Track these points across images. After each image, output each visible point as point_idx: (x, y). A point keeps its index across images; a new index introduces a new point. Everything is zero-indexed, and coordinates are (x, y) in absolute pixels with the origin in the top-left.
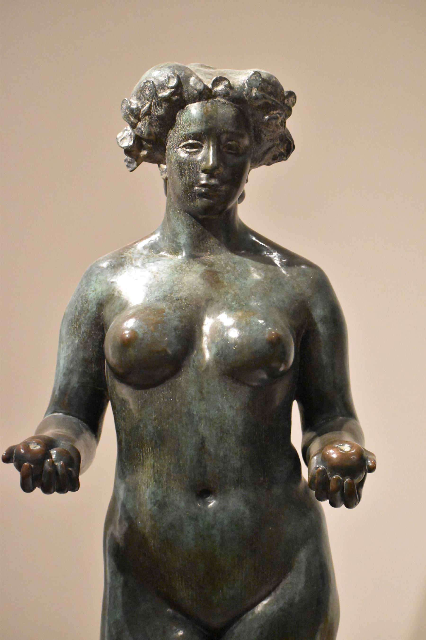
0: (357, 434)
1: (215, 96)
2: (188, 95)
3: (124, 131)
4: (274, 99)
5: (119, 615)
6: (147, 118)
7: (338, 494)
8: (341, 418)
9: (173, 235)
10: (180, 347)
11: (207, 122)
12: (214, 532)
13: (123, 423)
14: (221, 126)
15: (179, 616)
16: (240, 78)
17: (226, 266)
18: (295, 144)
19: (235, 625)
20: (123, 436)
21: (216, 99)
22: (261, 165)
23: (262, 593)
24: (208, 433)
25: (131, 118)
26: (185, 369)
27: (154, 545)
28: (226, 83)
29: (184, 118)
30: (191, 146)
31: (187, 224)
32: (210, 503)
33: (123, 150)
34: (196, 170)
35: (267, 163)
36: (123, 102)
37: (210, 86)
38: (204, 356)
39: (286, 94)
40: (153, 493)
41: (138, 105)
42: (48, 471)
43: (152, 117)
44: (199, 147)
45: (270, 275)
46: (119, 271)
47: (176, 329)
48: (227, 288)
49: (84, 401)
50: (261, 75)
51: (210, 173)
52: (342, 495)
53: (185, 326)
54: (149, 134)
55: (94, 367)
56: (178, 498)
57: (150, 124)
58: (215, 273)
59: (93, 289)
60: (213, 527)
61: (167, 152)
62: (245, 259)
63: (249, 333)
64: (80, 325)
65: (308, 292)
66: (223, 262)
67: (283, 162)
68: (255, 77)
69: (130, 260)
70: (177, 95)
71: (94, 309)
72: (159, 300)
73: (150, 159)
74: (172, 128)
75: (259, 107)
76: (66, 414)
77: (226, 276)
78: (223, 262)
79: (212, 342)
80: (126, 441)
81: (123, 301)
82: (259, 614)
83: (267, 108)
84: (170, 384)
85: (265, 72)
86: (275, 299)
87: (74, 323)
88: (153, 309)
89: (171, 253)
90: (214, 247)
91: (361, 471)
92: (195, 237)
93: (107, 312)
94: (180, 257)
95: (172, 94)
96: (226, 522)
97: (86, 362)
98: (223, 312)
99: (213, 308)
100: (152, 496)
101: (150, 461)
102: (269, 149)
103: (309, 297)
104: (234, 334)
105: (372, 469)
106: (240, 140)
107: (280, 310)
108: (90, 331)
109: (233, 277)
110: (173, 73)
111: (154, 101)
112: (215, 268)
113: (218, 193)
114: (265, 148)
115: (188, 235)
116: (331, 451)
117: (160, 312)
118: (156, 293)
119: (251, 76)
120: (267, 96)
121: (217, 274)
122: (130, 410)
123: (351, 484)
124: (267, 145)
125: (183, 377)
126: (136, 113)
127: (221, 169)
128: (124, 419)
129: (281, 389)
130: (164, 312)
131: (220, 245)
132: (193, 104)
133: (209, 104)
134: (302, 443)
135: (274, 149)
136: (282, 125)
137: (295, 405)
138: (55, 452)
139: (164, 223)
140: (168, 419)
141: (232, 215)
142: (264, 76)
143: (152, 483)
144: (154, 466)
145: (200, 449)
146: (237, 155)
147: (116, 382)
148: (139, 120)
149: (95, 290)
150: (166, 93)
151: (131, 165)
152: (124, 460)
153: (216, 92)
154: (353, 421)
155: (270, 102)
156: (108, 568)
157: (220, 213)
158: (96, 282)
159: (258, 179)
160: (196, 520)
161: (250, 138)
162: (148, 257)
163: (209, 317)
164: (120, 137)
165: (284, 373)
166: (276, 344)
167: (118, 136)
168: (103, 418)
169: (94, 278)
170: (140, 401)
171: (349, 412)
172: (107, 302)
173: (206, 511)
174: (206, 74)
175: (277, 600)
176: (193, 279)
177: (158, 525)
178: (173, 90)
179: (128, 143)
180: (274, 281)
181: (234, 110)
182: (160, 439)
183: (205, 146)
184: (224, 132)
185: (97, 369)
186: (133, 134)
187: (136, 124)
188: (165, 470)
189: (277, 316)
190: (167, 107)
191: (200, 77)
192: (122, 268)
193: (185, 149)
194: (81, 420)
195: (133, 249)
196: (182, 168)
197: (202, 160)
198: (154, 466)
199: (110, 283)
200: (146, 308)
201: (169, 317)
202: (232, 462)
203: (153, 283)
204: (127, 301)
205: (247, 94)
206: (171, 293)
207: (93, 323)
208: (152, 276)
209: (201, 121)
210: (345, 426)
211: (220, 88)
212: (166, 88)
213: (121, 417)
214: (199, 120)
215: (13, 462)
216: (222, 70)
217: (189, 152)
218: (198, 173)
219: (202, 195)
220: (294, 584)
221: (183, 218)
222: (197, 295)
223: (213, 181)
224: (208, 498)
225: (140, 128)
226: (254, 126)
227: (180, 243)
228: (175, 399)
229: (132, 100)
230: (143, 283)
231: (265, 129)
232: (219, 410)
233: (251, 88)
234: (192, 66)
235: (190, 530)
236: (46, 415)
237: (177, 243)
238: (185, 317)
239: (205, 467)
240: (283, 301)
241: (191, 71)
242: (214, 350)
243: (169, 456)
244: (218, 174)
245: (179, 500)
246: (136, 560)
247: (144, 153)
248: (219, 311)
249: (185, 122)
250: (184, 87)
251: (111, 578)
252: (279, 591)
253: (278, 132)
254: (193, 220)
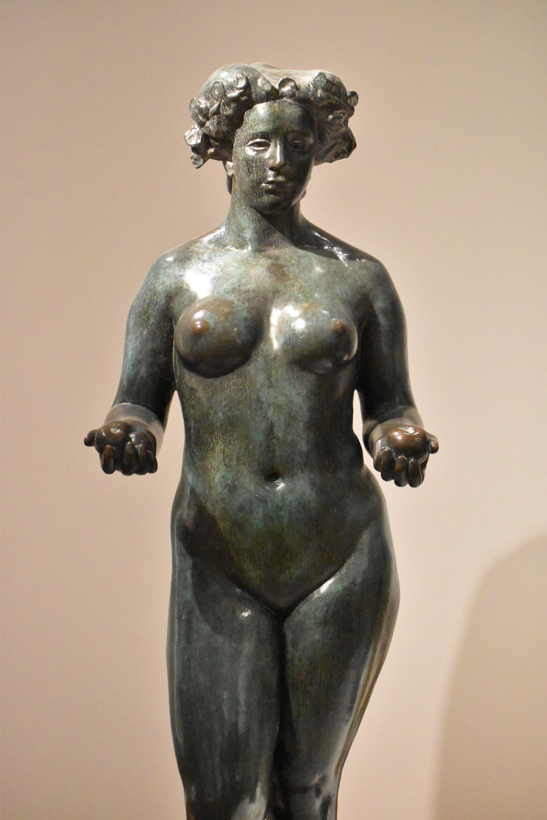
0: (416, 421)
2: (256, 95)
3: (191, 130)
4: (337, 99)
5: (189, 595)
6: (215, 117)
7: (403, 474)
8: (401, 407)
9: (239, 230)
10: (249, 337)
11: (274, 122)
12: (282, 513)
13: (192, 411)
14: (288, 125)
15: (247, 596)
16: (306, 78)
17: (291, 260)
18: (356, 142)
19: (301, 604)
20: (192, 423)
22: (323, 162)
23: (326, 574)
24: (276, 418)
25: (200, 117)
26: (254, 358)
27: (224, 527)
28: (293, 84)
29: (252, 118)
30: (259, 144)
32: (278, 486)
33: (191, 147)
35: (329, 160)
36: (192, 101)
37: (277, 87)
38: (272, 345)
39: (349, 94)
40: (223, 477)
41: (206, 105)
42: (125, 454)
43: (220, 117)
44: (266, 145)
45: (333, 268)
46: (186, 265)
47: (245, 319)
48: (292, 281)
49: (151, 390)
50: (325, 76)
51: (277, 170)
52: (407, 473)
53: (254, 317)
54: (217, 133)
55: (162, 358)
56: (248, 481)
57: (219, 123)
58: (281, 266)
59: (161, 282)
60: (281, 509)
61: (234, 149)
62: (309, 253)
63: (316, 323)
64: (148, 316)
65: (370, 285)
66: (287, 256)
67: (345, 159)
68: (320, 78)
69: (196, 255)
71: (163, 301)
72: (228, 293)
73: (216, 156)
74: (239, 127)
75: (324, 107)
76: (133, 403)
77: (291, 269)
78: (287, 256)
79: (280, 332)
80: (195, 428)
81: (192, 293)
82: (324, 593)
83: (331, 108)
84: (240, 372)
85: (328, 73)
86: (338, 291)
87: (141, 315)
88: (223, 301)
89: (237, 248)
90: (279, 241)
91: (425, 453)
93: (176, 305)
94: (245, 251)
95: (241, 95)
96: (294, 504)
97: (154, 352)
98: (289, 304)
99: (280, 300)
100: (222, 480)
101: (220, 447)
102: (332, 147)
103: (371, 290)
104: (300, 325)
105: (435, 450)
106: (305, 139)
107: (344, 302)
108: (159, 322)
109: (298, 271)
110: (242, 75)
111: (223, 101)
112: (281, 262)
113: (284, 189)
114: (327, 147)
116: (396, 433)
117: (230, 304)
118: (224, 285)
119: (316, 77)
120: (332, 96)
121: (282, 268)
122: (200, 398)
123: (415, 464)
124: (330, 143)
125: (252, 365)
126: (204, 113)
127: (288, 167)
128: (193, 407)
129: (345, 377)
130: (233, 303)
131: (284, 240)
132: (260, 104)
133: (276, 105)
134: (363, 430)
135: (337, 147)
136: (345, 125)
137: (356, 393)
138: (133, 435)
139: (229, 218)
140: (238, 406)
141: (296, 209)
142: (328, 77)
143: (222, 467)
144: (224, 450)
145: (269, 435)
146: (303, 153)
147: (186, 371)
148: (208, 119)
149: (164, 283)
150: (234, 94)
151: (198, 162)
152: (193, 446)
153: (283, 93)
154: (412, 410)
155: (334, 102)
156: (176, 552)
157: (286, 208)
158: (164, 275)
159: (322, 176)
160: (265, 501)
161: (315, 136)
162: (214, 251)
163: (277, 308)
164: (188, 135)
165: (348, 362)
166: (342, 334)
167: (186, 134)
168: (169, 407)
169: (162, 272)
170: (210, 389)
171: (408, 402)
172: (176, 295)
173: (274, 494)
174: (271, 74)
175: (342, 579)
176: (258, 273)
177: (228, 507)
179: (196, 141)
180: (337, 274)
182: (232, 424)
183: (272, 144)
184: (291, 131)
185: (165, 359)
186: (200, 132)
187: (205, 123)
188: (234, 454)
189: (341, 307)
190: (236, 107)
191: (268, 78)
192: (189, 262)
193: (252, 147)
194: (150, 409)
195: (199, 243)
196: (250, 166)
197: (269, 158)
198: (224, 450)
199: (178, 276)
200: (215, 300)
201: (238, 308)
202: (299, 446)
203: (221, 276)
204: (196, 294)
205: (313, 95)
206: (239, 286)
207: (162, 316)
208: (220, 270)
209: (269, 121)
210: (405, 414)
211: (286, 89)
212: (235, 89)
213: (190, 405)
214: (267, 120)
215: (94, 445)
216: (287, 71)
217: (256, 151)
218: (265, 170)
219: (269, 192)
220: (356, 565)
221: (249, 213)
222: (264, 287)
223: (280, 178)
224: (276, 481)
225: (208, 127)
226: (319, 125)
227: (246, 237)
228: (245, 387)
229: (200, 100)
230: (213, 276)
231: (329, 128)
232: (286, 396)
233: (316, 88)
234: (257, 66)
235: (259, 512)
236: (114, 403)
237: (242, 237)
238: (252, 308)
239: (274, 451)
240: (347, 294)
241: (258, 72)
242: (282, 340)
243: (240, 441)
244: (284, 172)
245: (249, 484)
246: (204, 542)
247: (211, 150)
248: (286, 302)
249: (253, 122)
250: (252, 88)
251: (180, 561)
252: (343, 570)
253: (341, 131)
254: (259, 215)
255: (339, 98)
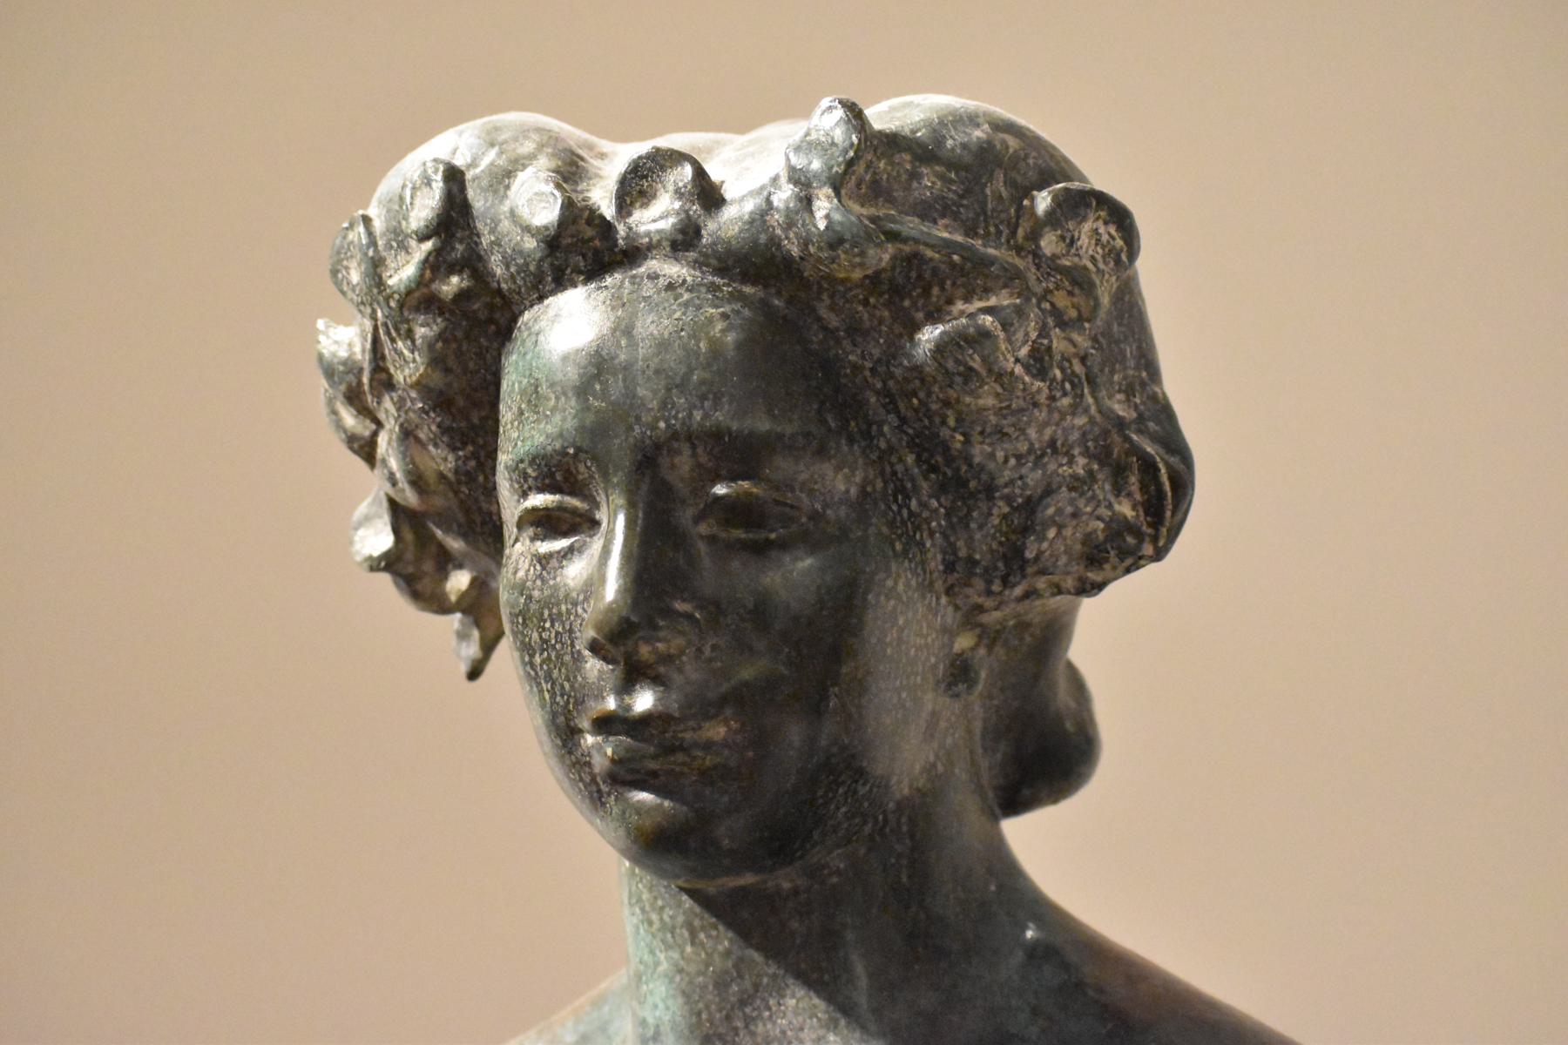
1: (632, 255)
21: (642, 269)
31: (663, 927)
34: (573, 646)
67: (1149, 573)
70: (452, 269)
92: (704, 987)
95: (436, 266)
115: (671, 981)
153: (631, 235)
178: (428, 245)
181: (725, 316)
190: (441, 336)
205: (790, 224)
218: (578, 658)
255: (971, 231)
